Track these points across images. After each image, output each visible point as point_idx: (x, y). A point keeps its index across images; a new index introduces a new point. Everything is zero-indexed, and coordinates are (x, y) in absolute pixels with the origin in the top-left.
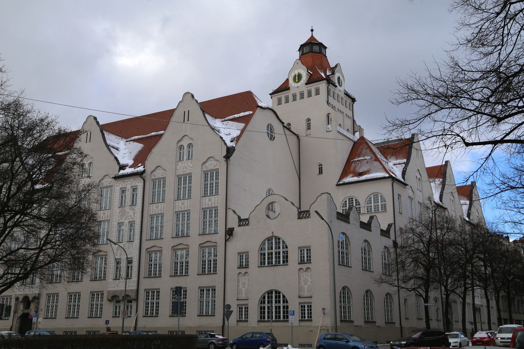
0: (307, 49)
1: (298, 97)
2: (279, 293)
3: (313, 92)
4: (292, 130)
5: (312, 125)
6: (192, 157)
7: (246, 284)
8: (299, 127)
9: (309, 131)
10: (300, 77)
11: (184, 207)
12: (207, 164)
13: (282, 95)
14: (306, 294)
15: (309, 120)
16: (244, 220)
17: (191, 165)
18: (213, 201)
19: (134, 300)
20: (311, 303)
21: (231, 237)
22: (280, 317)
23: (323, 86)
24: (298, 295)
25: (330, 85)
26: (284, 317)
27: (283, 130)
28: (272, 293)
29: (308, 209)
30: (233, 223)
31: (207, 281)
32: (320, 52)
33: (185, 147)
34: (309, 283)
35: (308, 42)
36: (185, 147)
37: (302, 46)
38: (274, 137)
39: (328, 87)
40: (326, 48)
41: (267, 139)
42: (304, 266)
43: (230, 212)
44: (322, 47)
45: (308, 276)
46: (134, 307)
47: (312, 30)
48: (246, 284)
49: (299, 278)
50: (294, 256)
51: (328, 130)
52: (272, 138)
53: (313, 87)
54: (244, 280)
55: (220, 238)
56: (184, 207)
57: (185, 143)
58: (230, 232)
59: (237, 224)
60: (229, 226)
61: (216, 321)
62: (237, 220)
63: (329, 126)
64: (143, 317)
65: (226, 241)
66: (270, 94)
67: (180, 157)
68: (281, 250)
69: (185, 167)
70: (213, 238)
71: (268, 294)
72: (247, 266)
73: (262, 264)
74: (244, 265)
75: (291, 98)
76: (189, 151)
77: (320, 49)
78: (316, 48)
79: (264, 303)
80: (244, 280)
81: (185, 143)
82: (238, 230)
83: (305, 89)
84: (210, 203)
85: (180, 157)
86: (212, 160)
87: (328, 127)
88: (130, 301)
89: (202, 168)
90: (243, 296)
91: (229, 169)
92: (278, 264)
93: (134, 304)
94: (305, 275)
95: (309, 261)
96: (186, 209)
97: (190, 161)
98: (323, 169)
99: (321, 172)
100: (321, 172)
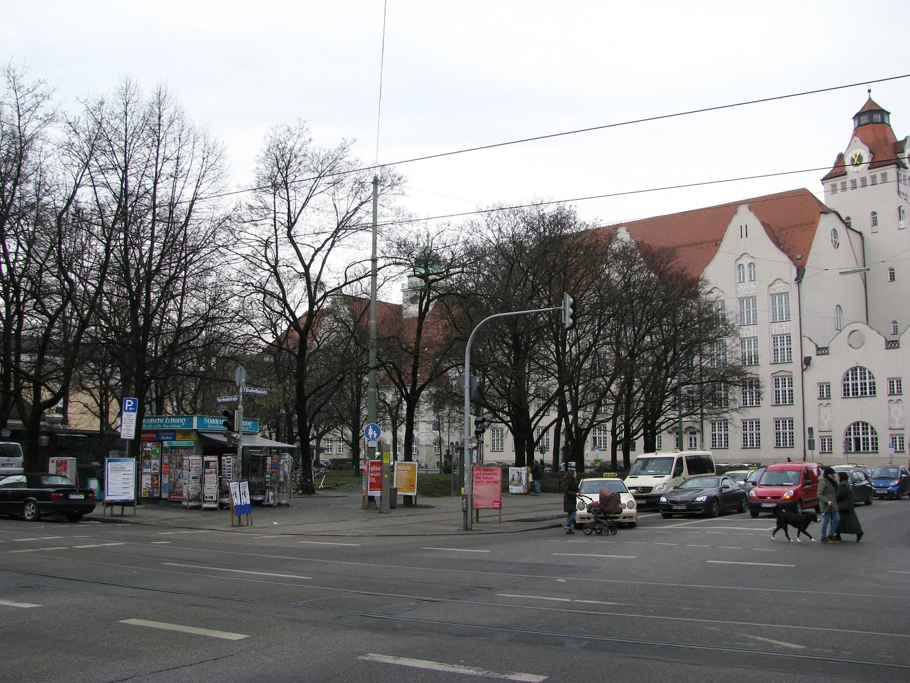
0: (864, 119)
1: (859, 183)
2: (867, 424)
3: (879, 179)
4: (852, 227)
5: (878, 219)
6: (754, 278)
7: (828, 415)
8: (861, 222)
9: (875, 227)
10: (859, 160)
11: (750, 334)
12: (774, 287)
13: (838, 182)
14: (897, 426)
15: (874, 213)
16: (823, 348)
17: (755, 287)
18: (784, 327)
19: (699, 431)
20: (903, 434)
21: (809, 367)
22: (868, 449)
23: (891, 171)
24: (888, 426)
25: (901, 168)
26: (873, 448)
27: (846, 232)
28: (858, 424)
29: (897, 339)
30: (810, 351)
31: (783, 412)
32: (883, 122)
33: (746, 267)
34: (900, 415)
35: (866, 110)
36: (746, 267)
37: (857, 116)
38: (838, 244)
39: (898, 172)
40: (888, 113)
41: (832, 246)
42: (895, 398)
43: (805, 340)
44: (884, 113)
45: (899, 408)
46: (698, 440)
47: (869, 91)
48: (828, 415)
49: (890, 410)
50: (882, 388)
51: (900, 227)
52: (837, 245)
53: (878, 172)
54: (826, 412)
55: (795, 367)
56: (750, 334)
57: (745, 261)
58: (807, 361)
59: (815, 353)
60: (805, 355)
61: (796, 452)
62: (815, 349)
63: (902, 222)
64: (820, 453)
65: (803, 370)
66: (822, 180)
67: (740, 277)
68: (867, 381)
69: (747, 288)
70: (787, 367)
71: (854, 425)
72: (829, 397)
73: (846, 394)
74: (825, 396)
75: (849, 185)
76: (750, 271)
77: (883, 118)
78: (877, 117)
79: (850, 434)
80: (826, 412)
81: (745, 261)
82: (816, 360)
83: (868, 174)
84: (781, 330)
85: (740, 277)
86: (779, 283)
87: (900, 223)
88: (694, 433)
89: (768, 291)
90: (826, 428)
91: (801, 293)
92: (864, 394)
93: (698, 436)
94: (895, 407)
95: (900, 392)
96: (752, 336)
97: (752, 283)
98: (895, 274)
99: (892, 277)
100: (892, 277)
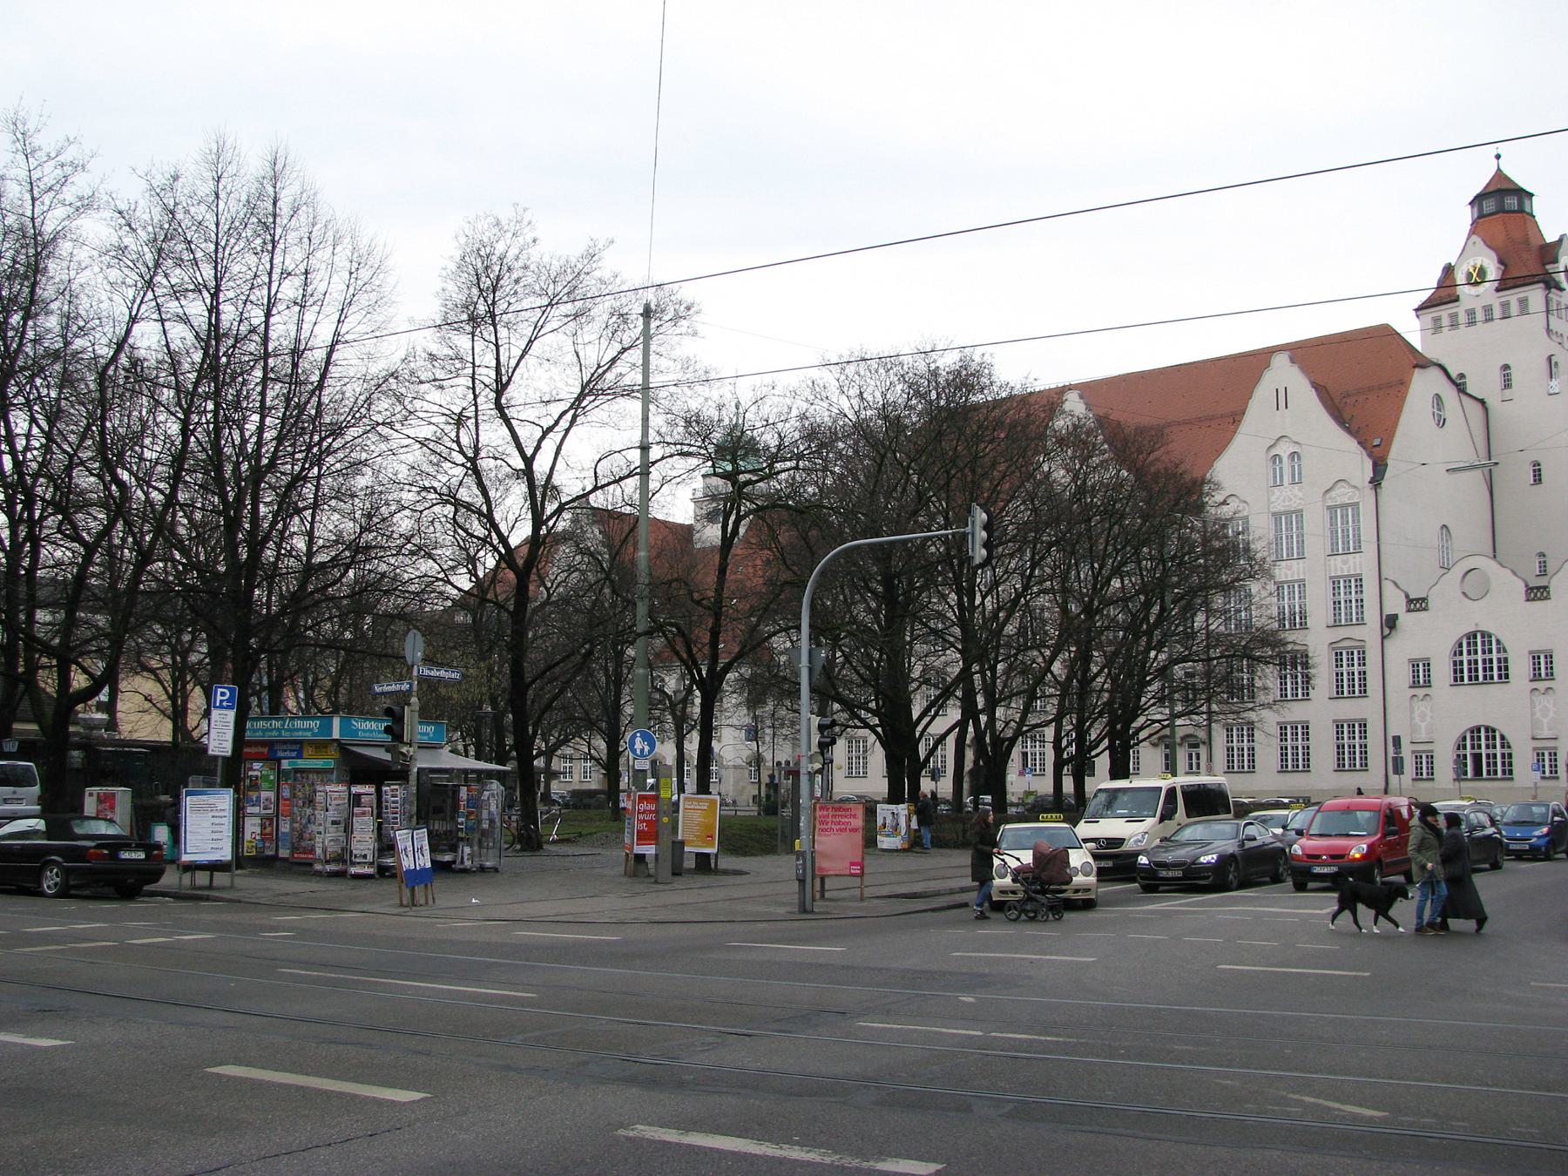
0: (1489, 206)
1: (1480, 316)
2: (1494, 731)
3: (1514, 309)
4: (1468, 391)
5: (1513, 377)
6: (1300, 478)
7: (1426, 715)
8: (1483, 383)
9: (1507, 391)
10: (1481, 275)
11: (1293, 574)
12: (1333, 494)
13: (1444, 313)
14: (1546, 733)
15: (1506, 367)
16: (1417, 600)
17: (1300, 494)
18: (1351, 563)
19: (1204, 743)
20: (1556, 748)
21: (1393, 632)
22: (1495, 772)
23: (1535, 295)
24: (1530, 733)
25: (1553, 290)
26: (1504, 772)
27: (1457, 399)
28: (1479, 731)
29: (1546, 584)
30: (1395, 604)
31: (1349, 709)
32: (1521, 211)
33: (1285, 459)
34: (1551, 714)
35: (1491, 189)
36: (1285, 459)
37: (1478, 200)
38: (1444, 420)
39: (1547, 297)
40: (1531, 195)
41: (1433, 423)
42: (1541, 685)
43: (1388, 586)
44: (1523, 195)
45: (1549, 702)
46: (1203, 758)
47: (1498, 157)
48: (1426, 715)
49: (1533, 706)
50: (1520, 668)
51: (1551, 391)
52: (1442, 422)
53: (1513, 297)
54: (1423, 709)
55: (1369, 632)
56: (1293, 574)
57: (1284, 450)
58: (1390, 622)
59: (1405, 608)
60: (1388, 611)
61: (1372, 779)
62: (1405, 601)
63: (1554, 383)
64: (1414, 780)
65: (1383, 638)
66: (1416, 310)
67: (1275, 477)
68: (1494, 656)
69: (1287, 497)
70: (1356, 632)
71: (1472, 732)
72: (1428, 684)
73: (1458, 678)
74: (1421, 681)
75: (1463, 318)
76: (1293, 467)
77: (1521, 204)
78: (1511, 202)
79: (1465, 747)
80: (1423, 709)
81: (1284, 450)
82: (1405, 619)
83: (1495, 300)
84: (1345, 568)
85: (1275, 477)
86: (1343, 487)
87: (1552, 384)
88: (1196, 746)
89: (1324, 501)
90: (1423, 737)
91: (1380, 504)
92: (1488, 679)
93: (1203, 750)
94: (1542, 701)
95: (1550, 676)
96: (1296, 578)
97: (1296, 487)
98: (1542, 472)
99: (1538, 478)
100: (1538, 478)
